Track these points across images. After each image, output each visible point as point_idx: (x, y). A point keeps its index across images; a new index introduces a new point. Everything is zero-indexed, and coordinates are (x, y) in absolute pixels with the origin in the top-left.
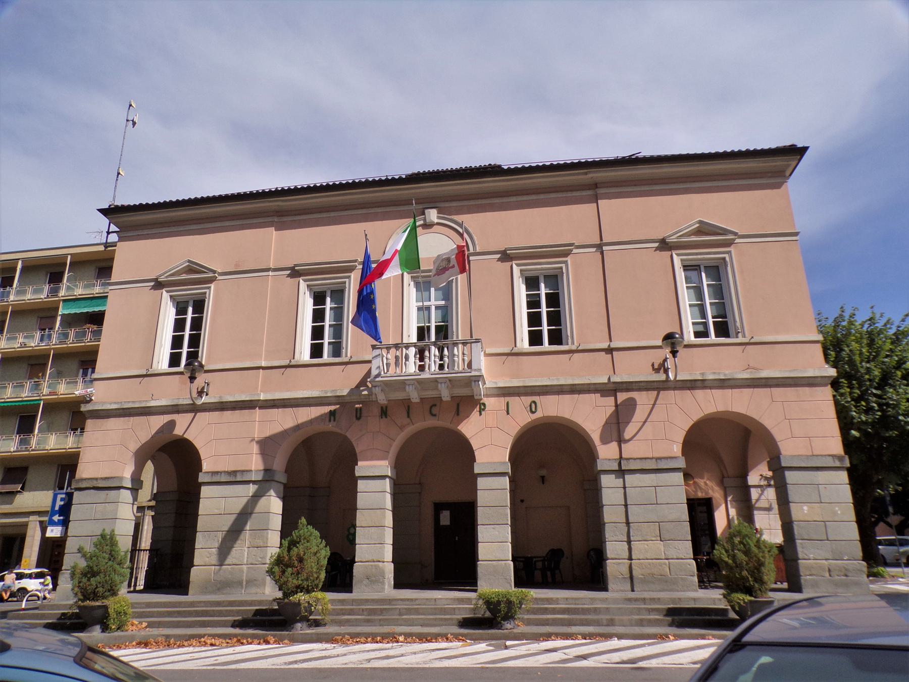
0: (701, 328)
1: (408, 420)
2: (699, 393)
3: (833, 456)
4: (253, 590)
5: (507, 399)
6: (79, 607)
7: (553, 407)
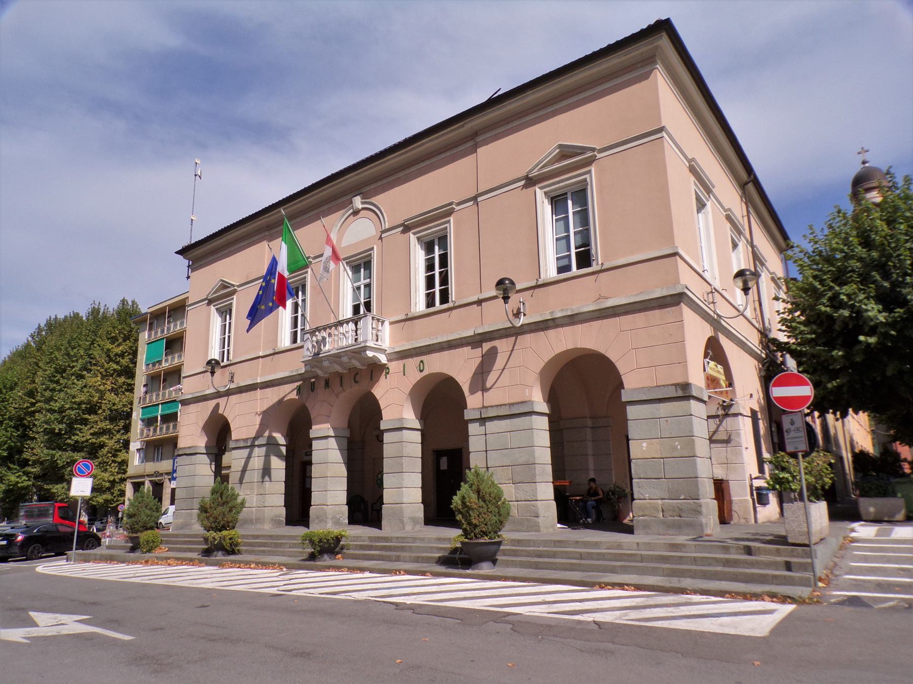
0: (564, 262)
1: (340, 389)
2: (551, 333)
3: (676, 385)
4: (259, 526)
5: (405, 361)
6: (462, 543)
7: (437, 364)
